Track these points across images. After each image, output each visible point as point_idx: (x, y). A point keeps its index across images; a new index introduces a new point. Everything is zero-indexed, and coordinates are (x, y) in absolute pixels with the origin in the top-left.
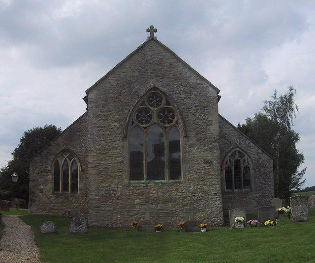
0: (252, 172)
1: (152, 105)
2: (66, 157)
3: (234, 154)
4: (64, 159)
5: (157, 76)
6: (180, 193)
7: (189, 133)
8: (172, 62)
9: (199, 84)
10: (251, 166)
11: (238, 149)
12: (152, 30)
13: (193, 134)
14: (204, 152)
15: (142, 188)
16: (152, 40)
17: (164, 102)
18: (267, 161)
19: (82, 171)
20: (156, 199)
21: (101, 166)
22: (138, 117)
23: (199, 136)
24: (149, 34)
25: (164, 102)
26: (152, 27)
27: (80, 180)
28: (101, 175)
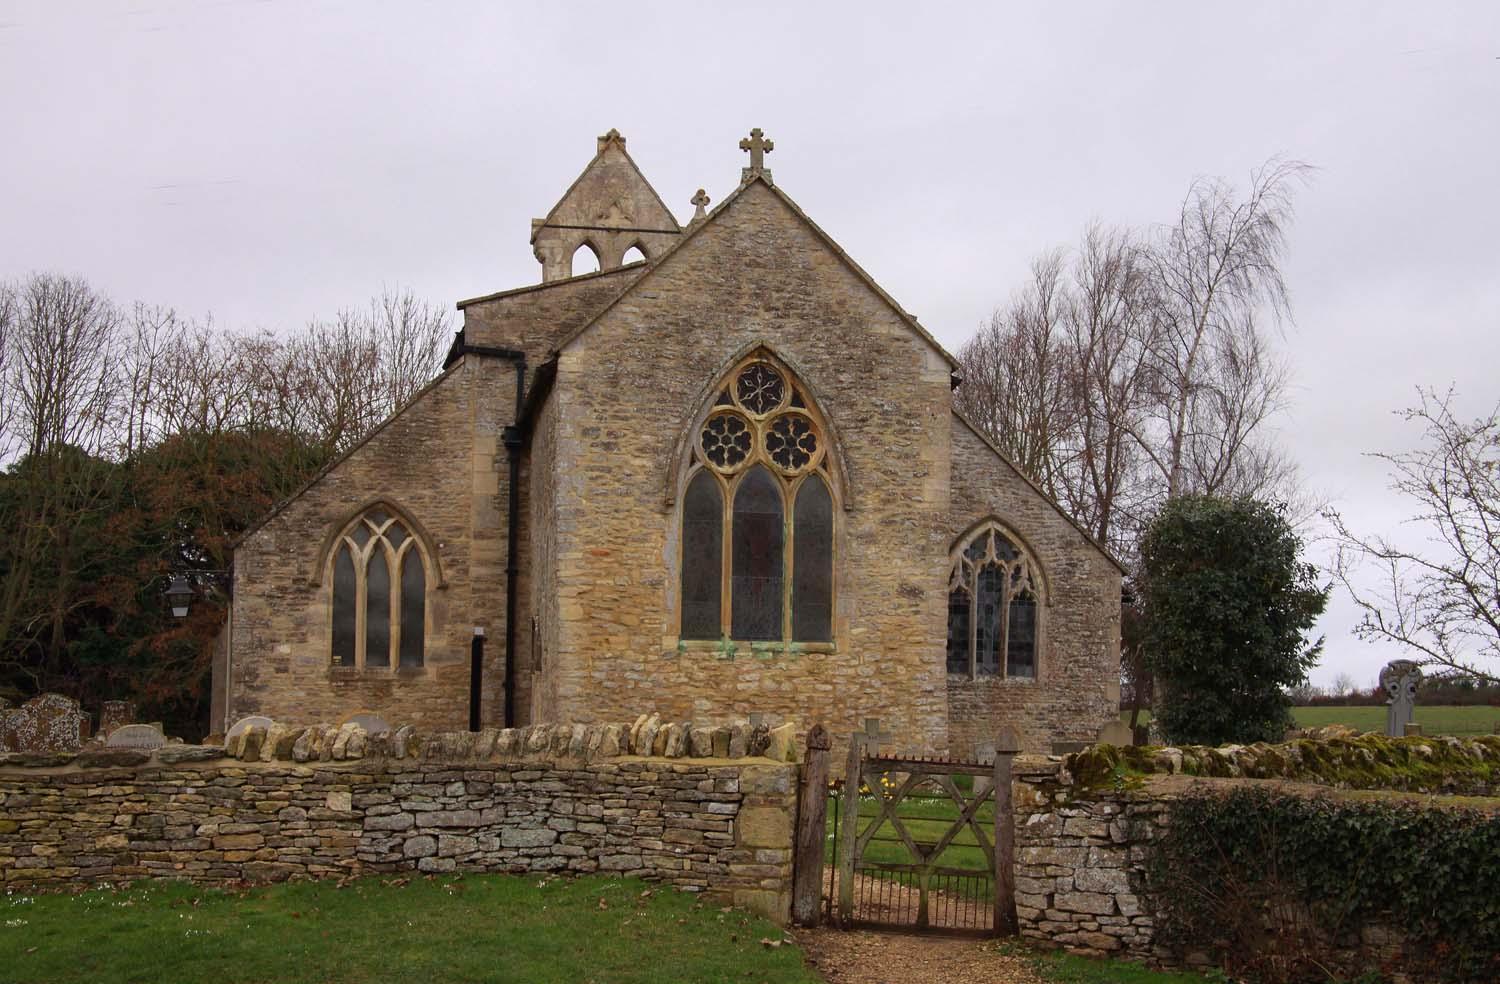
0: (1043, 616)
1: (752, 404)
2: (380, 531)
3: (978, 548)
4: (373, 540)
5: (768, 309)
6: (826, 683)
7: (859, 498)
8: (812, 260)
9: (898, 340)
10: (1040, 597)
11: (999, 527)
12: (757, 145)
13: (870, 501)
14: (903, 559)
15: (717, 664)
16: (757, 181)
17: (787, 395)
18: (1100, 578)
19: (443, 588)
20: (756, 699)
21: (598, 595)
22: (709, 439)
23: (891, 509)
24: (746, 159)
25: (787, 395)
26: (757, 133)
27: (436, 622)
28: (597, 622)
